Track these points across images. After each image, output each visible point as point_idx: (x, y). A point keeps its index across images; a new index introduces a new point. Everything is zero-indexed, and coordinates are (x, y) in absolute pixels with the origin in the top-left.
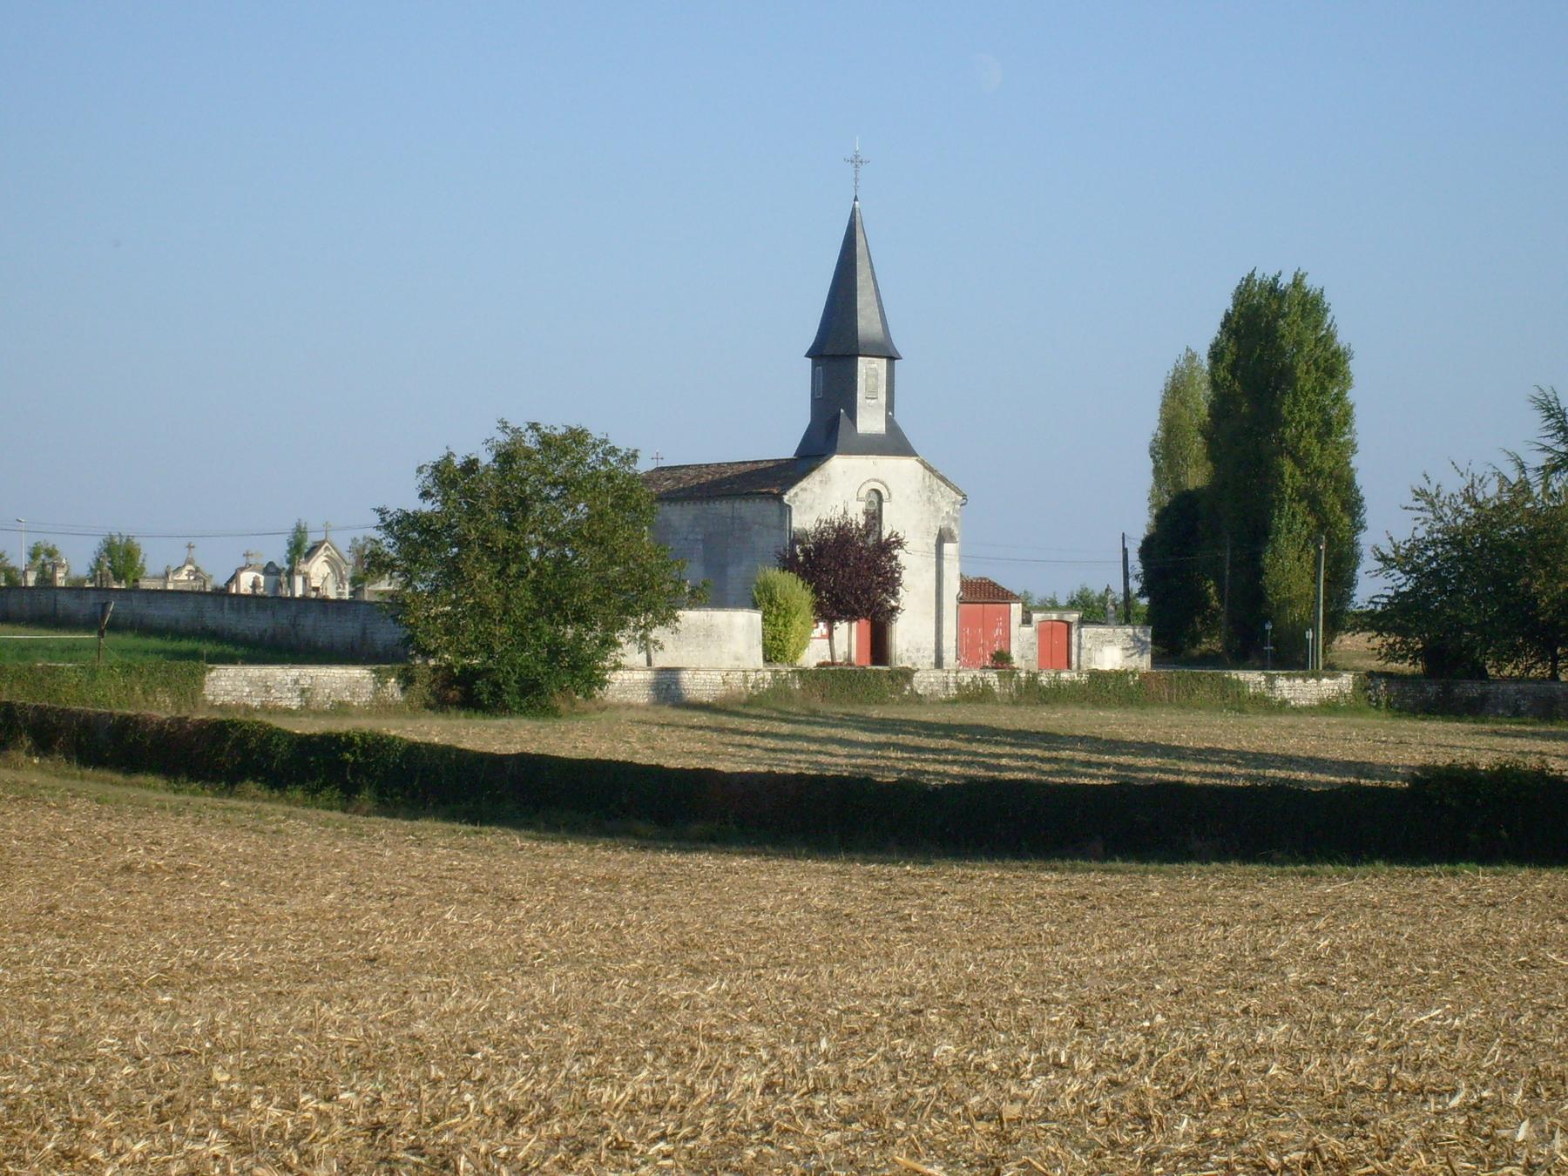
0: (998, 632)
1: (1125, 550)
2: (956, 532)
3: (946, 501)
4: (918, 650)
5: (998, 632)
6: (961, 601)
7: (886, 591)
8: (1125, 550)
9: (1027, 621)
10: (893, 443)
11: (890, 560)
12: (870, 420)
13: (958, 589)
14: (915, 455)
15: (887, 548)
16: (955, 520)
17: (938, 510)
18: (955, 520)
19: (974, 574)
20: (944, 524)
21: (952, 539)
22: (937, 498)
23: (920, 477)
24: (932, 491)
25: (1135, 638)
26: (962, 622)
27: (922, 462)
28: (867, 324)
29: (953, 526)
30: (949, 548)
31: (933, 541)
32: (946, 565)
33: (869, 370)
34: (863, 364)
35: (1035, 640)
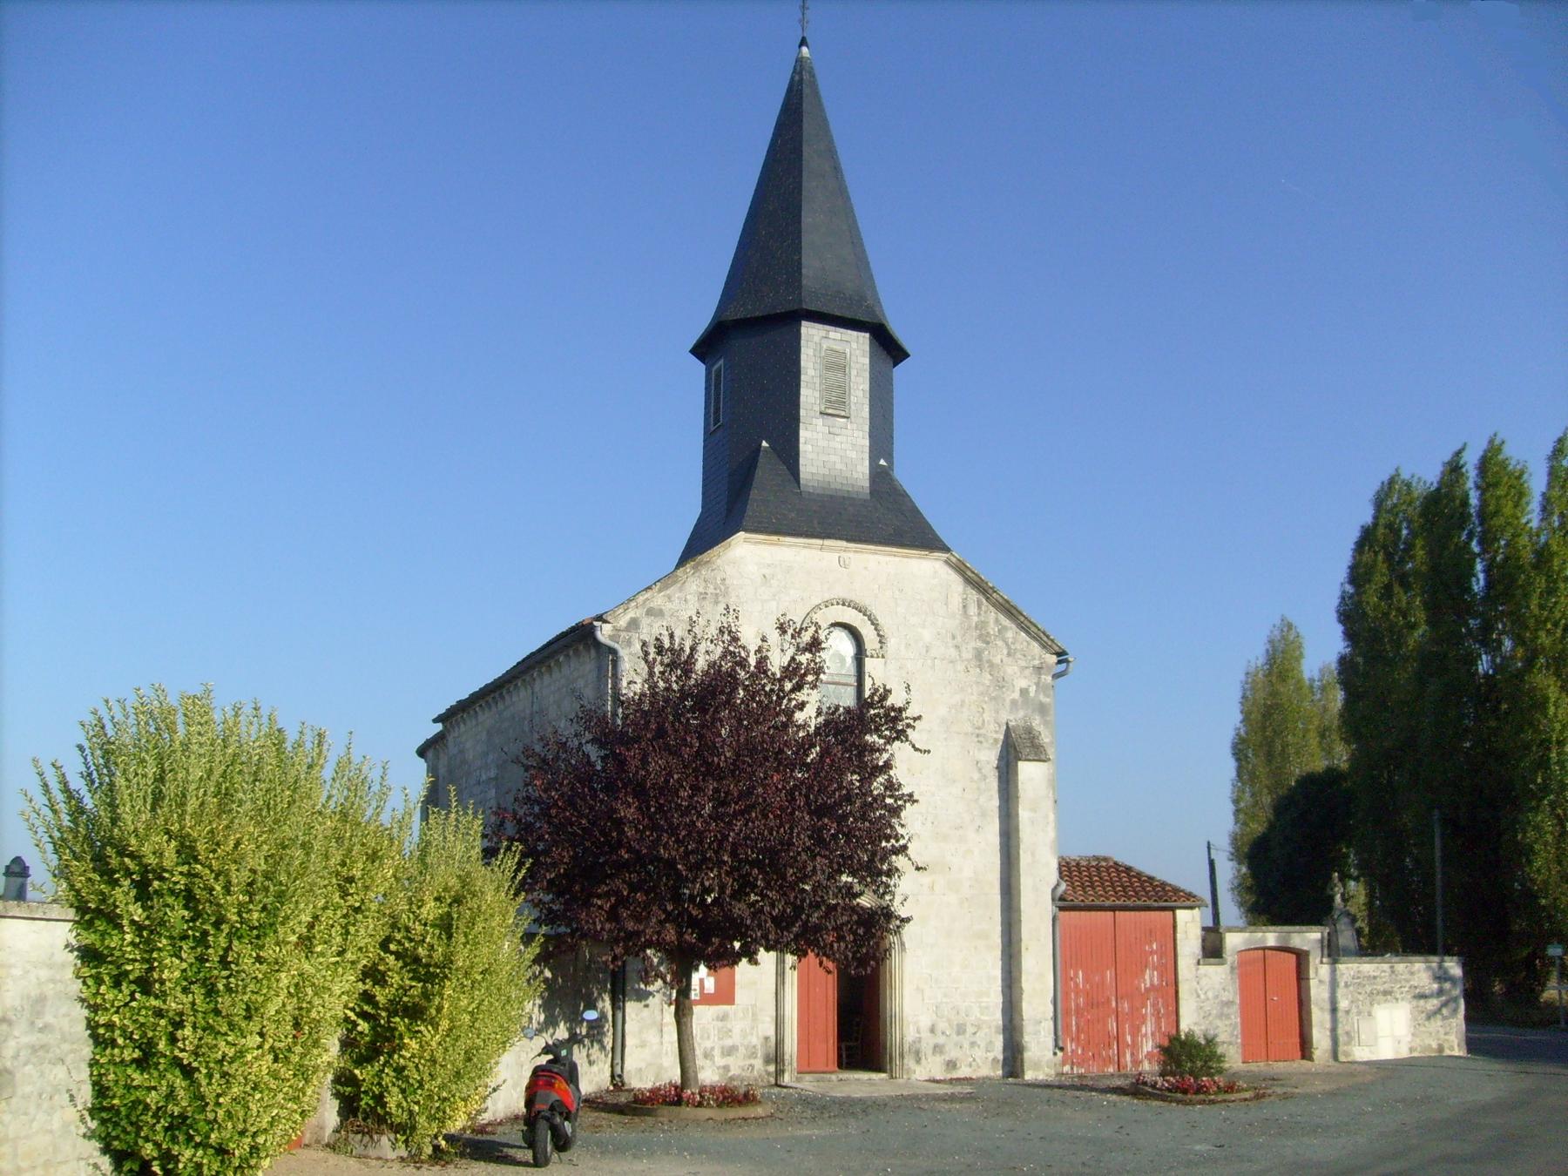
0: (1150, 978)
1: (1212, 863)
2: (1046, 738)
3: (1021, 663)
4: (961, 1030)
5: (1150, 978)
6: (1063, 904)
7: (847, 864)
8: (1212, 863)
9: (1212, 950)
10: (883, 516)
11: (867, 778)
12: (832, 448)
13: (1052, 875)
14: (946, 549)
15: (866, 724)
16: (1042, 709)
17: (1001, 683)
18: (1042, 709)
19: (1082, 850)
20: (1016, 718)
21: (1038, 753)
22: (998, 655)
23: (956, 601)
24: (984, 638)
25: (1442, 977)
26: (1066, 958)
27: (960, 569)
28: (817, 265)
29: (1037, 723)
30: (1030, 773)
31: (991, 756)
32: (1024, 814)
33: (829, 356)
34: (813, 337)
35: (1232, 994)
